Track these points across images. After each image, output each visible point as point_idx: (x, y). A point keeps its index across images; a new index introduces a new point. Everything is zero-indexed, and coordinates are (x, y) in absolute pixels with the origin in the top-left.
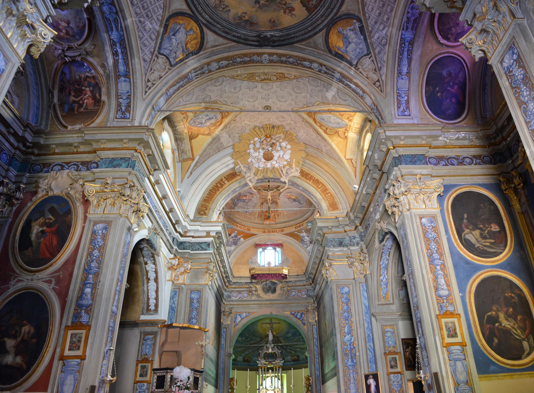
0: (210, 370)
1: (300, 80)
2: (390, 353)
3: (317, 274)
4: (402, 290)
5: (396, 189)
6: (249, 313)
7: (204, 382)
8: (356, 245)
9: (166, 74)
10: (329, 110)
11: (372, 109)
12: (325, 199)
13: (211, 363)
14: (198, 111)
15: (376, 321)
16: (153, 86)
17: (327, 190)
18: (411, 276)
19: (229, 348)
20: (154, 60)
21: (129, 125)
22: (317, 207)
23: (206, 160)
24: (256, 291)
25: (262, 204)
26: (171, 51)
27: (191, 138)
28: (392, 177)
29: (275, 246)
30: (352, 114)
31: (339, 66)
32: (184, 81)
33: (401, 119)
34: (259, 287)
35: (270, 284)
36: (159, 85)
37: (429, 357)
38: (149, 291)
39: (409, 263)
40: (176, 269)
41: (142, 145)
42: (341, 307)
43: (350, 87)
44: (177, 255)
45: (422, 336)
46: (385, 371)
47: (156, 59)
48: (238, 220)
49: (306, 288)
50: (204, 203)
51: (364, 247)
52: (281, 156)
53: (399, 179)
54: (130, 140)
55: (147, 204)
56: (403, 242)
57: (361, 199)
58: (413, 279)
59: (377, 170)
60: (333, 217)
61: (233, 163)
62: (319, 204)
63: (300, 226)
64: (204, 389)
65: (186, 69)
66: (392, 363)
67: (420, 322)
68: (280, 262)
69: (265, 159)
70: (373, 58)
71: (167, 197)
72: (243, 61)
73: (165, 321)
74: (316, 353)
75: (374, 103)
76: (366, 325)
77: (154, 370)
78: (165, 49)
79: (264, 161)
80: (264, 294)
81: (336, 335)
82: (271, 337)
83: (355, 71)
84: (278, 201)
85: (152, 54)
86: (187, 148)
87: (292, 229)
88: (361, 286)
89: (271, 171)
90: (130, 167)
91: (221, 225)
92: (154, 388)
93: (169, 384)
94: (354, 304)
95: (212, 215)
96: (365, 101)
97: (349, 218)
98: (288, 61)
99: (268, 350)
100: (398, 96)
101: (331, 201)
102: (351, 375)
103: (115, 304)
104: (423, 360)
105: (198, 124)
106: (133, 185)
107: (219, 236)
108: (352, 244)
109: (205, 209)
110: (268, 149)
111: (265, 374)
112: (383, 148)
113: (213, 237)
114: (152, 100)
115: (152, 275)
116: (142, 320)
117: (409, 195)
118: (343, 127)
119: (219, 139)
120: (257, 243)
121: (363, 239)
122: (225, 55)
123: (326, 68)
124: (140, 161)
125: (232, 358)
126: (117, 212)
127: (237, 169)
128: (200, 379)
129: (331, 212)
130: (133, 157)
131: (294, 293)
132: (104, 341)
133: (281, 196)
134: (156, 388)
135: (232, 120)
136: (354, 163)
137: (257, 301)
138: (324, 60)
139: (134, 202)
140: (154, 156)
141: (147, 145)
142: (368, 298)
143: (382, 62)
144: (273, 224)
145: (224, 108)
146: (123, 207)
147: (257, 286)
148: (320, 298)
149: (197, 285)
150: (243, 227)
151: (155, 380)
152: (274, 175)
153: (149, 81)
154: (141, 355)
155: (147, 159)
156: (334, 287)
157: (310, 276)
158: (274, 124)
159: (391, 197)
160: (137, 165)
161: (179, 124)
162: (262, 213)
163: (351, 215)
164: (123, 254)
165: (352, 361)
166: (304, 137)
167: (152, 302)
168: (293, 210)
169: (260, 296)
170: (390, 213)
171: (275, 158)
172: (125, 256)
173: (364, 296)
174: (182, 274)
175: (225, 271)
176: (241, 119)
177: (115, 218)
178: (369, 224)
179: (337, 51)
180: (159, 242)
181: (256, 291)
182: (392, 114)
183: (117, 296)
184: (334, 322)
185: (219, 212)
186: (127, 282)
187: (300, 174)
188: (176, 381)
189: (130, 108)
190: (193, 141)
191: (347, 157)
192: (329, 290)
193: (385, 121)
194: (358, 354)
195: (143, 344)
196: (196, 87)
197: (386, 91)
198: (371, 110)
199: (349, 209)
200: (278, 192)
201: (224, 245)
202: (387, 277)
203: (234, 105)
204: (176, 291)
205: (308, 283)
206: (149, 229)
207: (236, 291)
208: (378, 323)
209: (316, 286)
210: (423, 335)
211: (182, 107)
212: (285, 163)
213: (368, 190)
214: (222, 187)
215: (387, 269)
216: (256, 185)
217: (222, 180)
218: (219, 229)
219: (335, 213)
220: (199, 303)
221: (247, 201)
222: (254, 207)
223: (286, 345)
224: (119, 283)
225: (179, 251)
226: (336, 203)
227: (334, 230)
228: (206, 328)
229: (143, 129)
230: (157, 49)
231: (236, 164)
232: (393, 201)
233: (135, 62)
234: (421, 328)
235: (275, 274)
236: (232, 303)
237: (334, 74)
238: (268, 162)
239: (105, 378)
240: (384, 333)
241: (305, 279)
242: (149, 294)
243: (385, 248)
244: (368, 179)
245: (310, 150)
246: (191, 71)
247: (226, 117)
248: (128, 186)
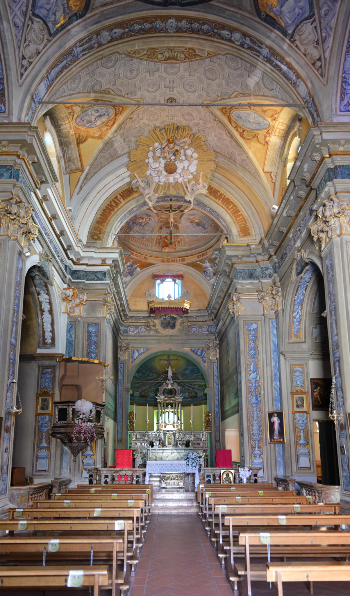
0: (110, 404)
1: (215, 58)
2: (297, 392)
3: (221, 309)
4: (316, 328)
5: (327, 210)
6: (147, 348)
7: (106, 416)
8: (268, 277)
9: (44, 47)
10: (249, 103)
11: (306, 102)
12: (236, 223)
13: (110, 398)
14: (87, 103)
15: (285, 360)
16: (30, 66)
17: (238, 211)
18: (333, 312)
19: (126, 383)
20: (28, 25)
21: (6, 121)
22: (225, 232)
23: (97, 172)
24: (154, 326)
25: (161, 228)
26: (48, 11)
27: (79, 142)
28: (323, 195)
29: (175, 277)
30: (278, 109)
31: (269, 37)
32: (69, 59)
33: (344, 116)
34: (157, 322)
35: (169, 319)
36: (37, 65)
37: (345, 397)
38: (44, 324)
39: (332, 298)
40: (71, 301)
41: (25, 149)
42: (247, 344)
43: (280, 70)
44: (71, 285)
45: (338, 376)
46: (291, 410)
47: (30, 23)
48: (134, 247)
49: (207, 324)
50: (97, 225)
51: (277, 279)
52: (186, 168)
53: (332, 197)
54: (11, 142)
55: (35, 223)
56: (328, 273)
57: (279, 222)
58: (335, 316)
59: (304, 186)
60: (244, 245)
61: (129, 176)
62: (228, 229)
63: (203, 255)
64: (105, 422)
65: (69, 40)
66: (299, 403)
67: (339, 361)
68: (180, 296)
69: (167, 172)
70: (317, 23)
71: (57, 217)
72: (142, 29)
73: (63, 355)
74: (216, 390)
75: (309, 93)
76: (273, 364)
77: (55, 403)
78: (41, 7)
79: (166, 174)
80: (162, 329)
81: (240, 373)
82: (170, 374)
83: (289, 45)
84: (180, 225)
85: (25, 15)
86: (74, 156)
87: (194, 259)
88: (271, 323)
89: (174, 187)
90: (14, 178)
91: (118, 251)
92: (57, 420)
93: (71, 416)
94: (262, 341)
95: (107, 240)
96: (299, 90)
97: (263, 246)
98: (201, 29)
99: (168, 386)
100: (343, 82)
101: (242, 226)
102: (255, 413)
103: (13, 336)
104: (337, 400)
105: (87, 123)
106: (19, 200)
107: (116, 265)
108: (264, 276)
109: (98, 232)
110: (170, 158)
111: (164, 409)
112: (316, 156)
113: (109, 265)
114: (30, 86)
115: (46, 307)
116: (39, 354)
117: (342, 218)
118: (264, 129)
119: (112, 145)
120: (155, 274)
121: (277, 270)
122: (119, 19)
123: (251, 40)
124: (25, 171)
125: (130, 393)
126: (5, 234)
127: (134, 184)
128: (102, 412)
129: (242, 239)
130: (15, 165)
131: (194, 329)
132: (6, 374)
133: (182, 219)
134: (59, 421)
135: (128, 118)
136: (274, 177)
137: (155, 336)
138: (249, 27)
139: (23, 221)
140: (40, 165)
141: (31, 150)
142: (277, 336)
143: (328, 29)
144: (172, 252)
145: (118, 100)
146: (11, 228)
147: (155, 321)
148: (223, 334)
149: (94, 319)
150: (139, 255)
151: (57, 413)
152: (177, 192)
153: (24, 58)
154: (41, 389)
155: (31, 168)
156: (241, 323)
157: (213, 311)
158: (178, 125)
159: (319, 219)
160: (21, 175)
161: (63, 123)
162: (161, 239)
163: (266, 242)
164: (17, 282)
165: (257, 399)
166: (214, 142)
167: (48, 335)
168: (196, 236)
169: (158, 331)
170: (315, 239)
171: (179, 171)
172: (18, 284)
173: (273, 334)
174: (77, 305)
175: (121, 303)
176: (138, 116)
177: (3, 240)
178: (286, 253)
179: (268, 12)
180: (52, 270)
181: (154, 326)
182: (332, 109)
183: (14, 328)
184: (240, 360)
185: (114, 236)
186: (24, 313)
187: (207, 191)
188: (79, 414)
189: (4, 97)
190: (81, 146)
191: (265, 171)
192: (233, 327)
193: (322, 119)
194: (262, 392)
195: (42, 378)
196: (82, 69)
197: (328, 74)
198: (305, 103)
199: (263, 235)
200: (181, 213)
201: (120, 275)
202: (300, 314)
203: (130, 96)
204: (73, 324)
205: (211, 318)
206: (40, 254)
208: (287, 362)
209: (219, 322)
210: (340, 375)
211: (67, 97)
212: (191, 177)
213: (290, 211)
214: (116, 206)
215: (302, 305)
216: (156, 205)
217: (116, 197)
218: (116, 256)
219: (246, 240)
220: (98, 337)
221: (143, 224)
222: (152, 232)
223: (183, 382)
224: (16, 314)
225: (73, 280)
226: (248, 228)
227: (245, 259)
228: (105, 363)
229: (25, 127)
230: (30, 8)
231: (132, 177)
232: (321, 225)
233: (3, 28)
234: (339, 367)
235: (176, 309)
236: (129, 338)
237: (261, 50)
238: (170, 175)
239: (11, 410)
240: (292, 372)
241: (207, 314)
242: (44, 327)
243: (302, 281)
244: (292, 198)
245: (221, 159)
246: (76, 44)
247: (121, 113)
248: (14, 201)
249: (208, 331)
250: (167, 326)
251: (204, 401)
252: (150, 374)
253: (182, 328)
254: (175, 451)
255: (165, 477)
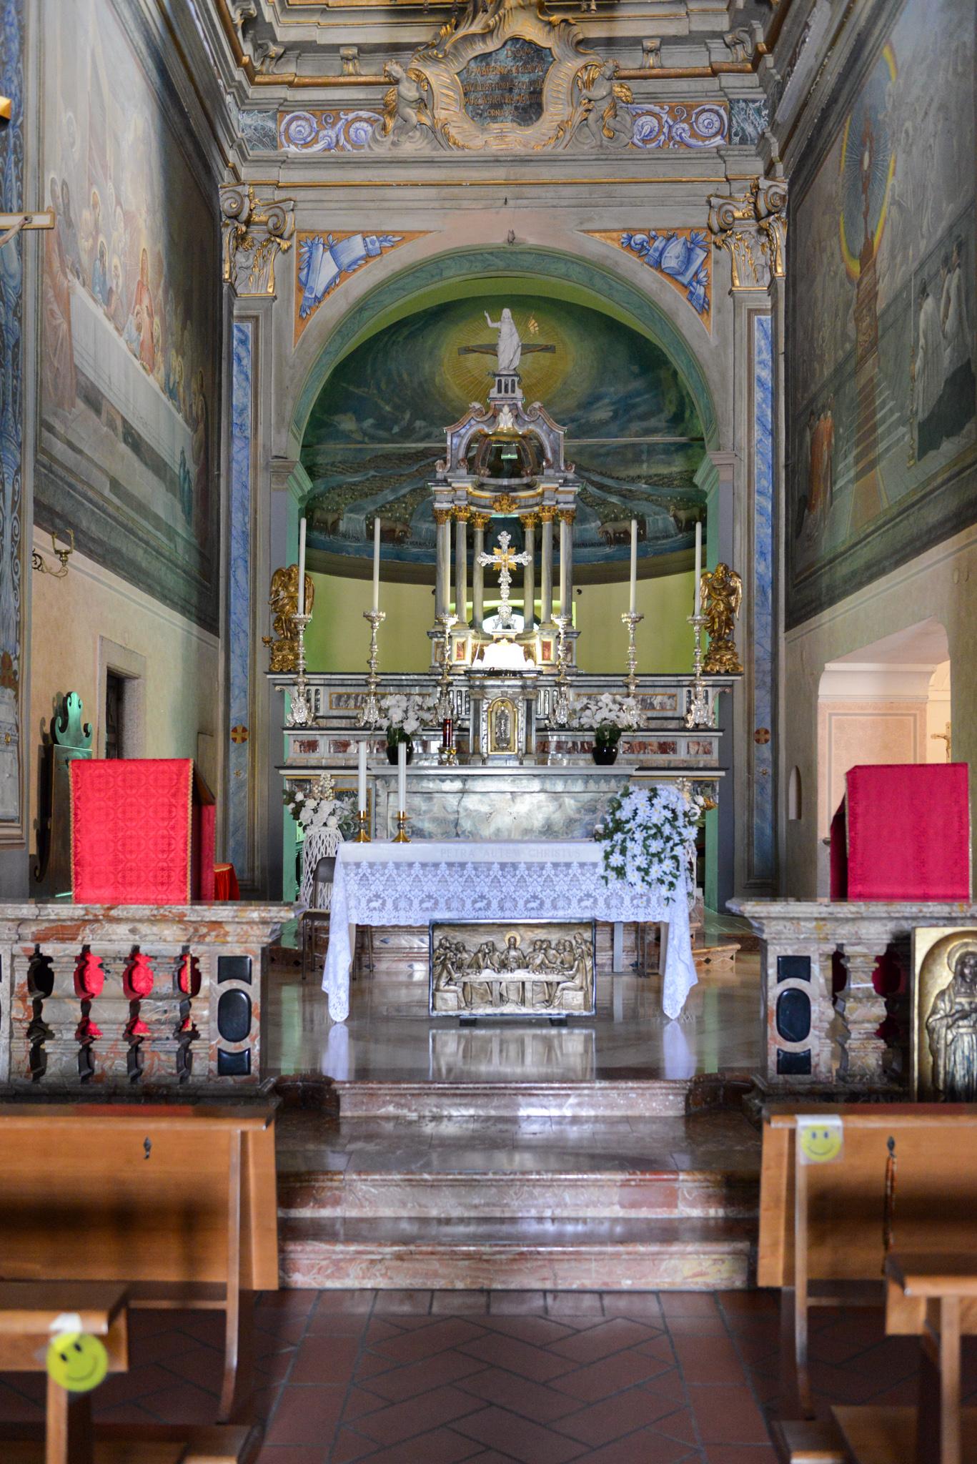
6: (383, 235)
34: (441, 78)
35: (505, 61)
80: (468, 126)
131: (648, 123)
137: (430, 162)
147: (430, 72)
169: (447, 136)
181: (422, 104)
207: (304, 105)
236: (285, 176)
249: (727, 132)
250: (498, 106)
251: (681, 554)
252: (418, 424)
253: (577, 119)
254: (536, 785)
255: (460, 948)
